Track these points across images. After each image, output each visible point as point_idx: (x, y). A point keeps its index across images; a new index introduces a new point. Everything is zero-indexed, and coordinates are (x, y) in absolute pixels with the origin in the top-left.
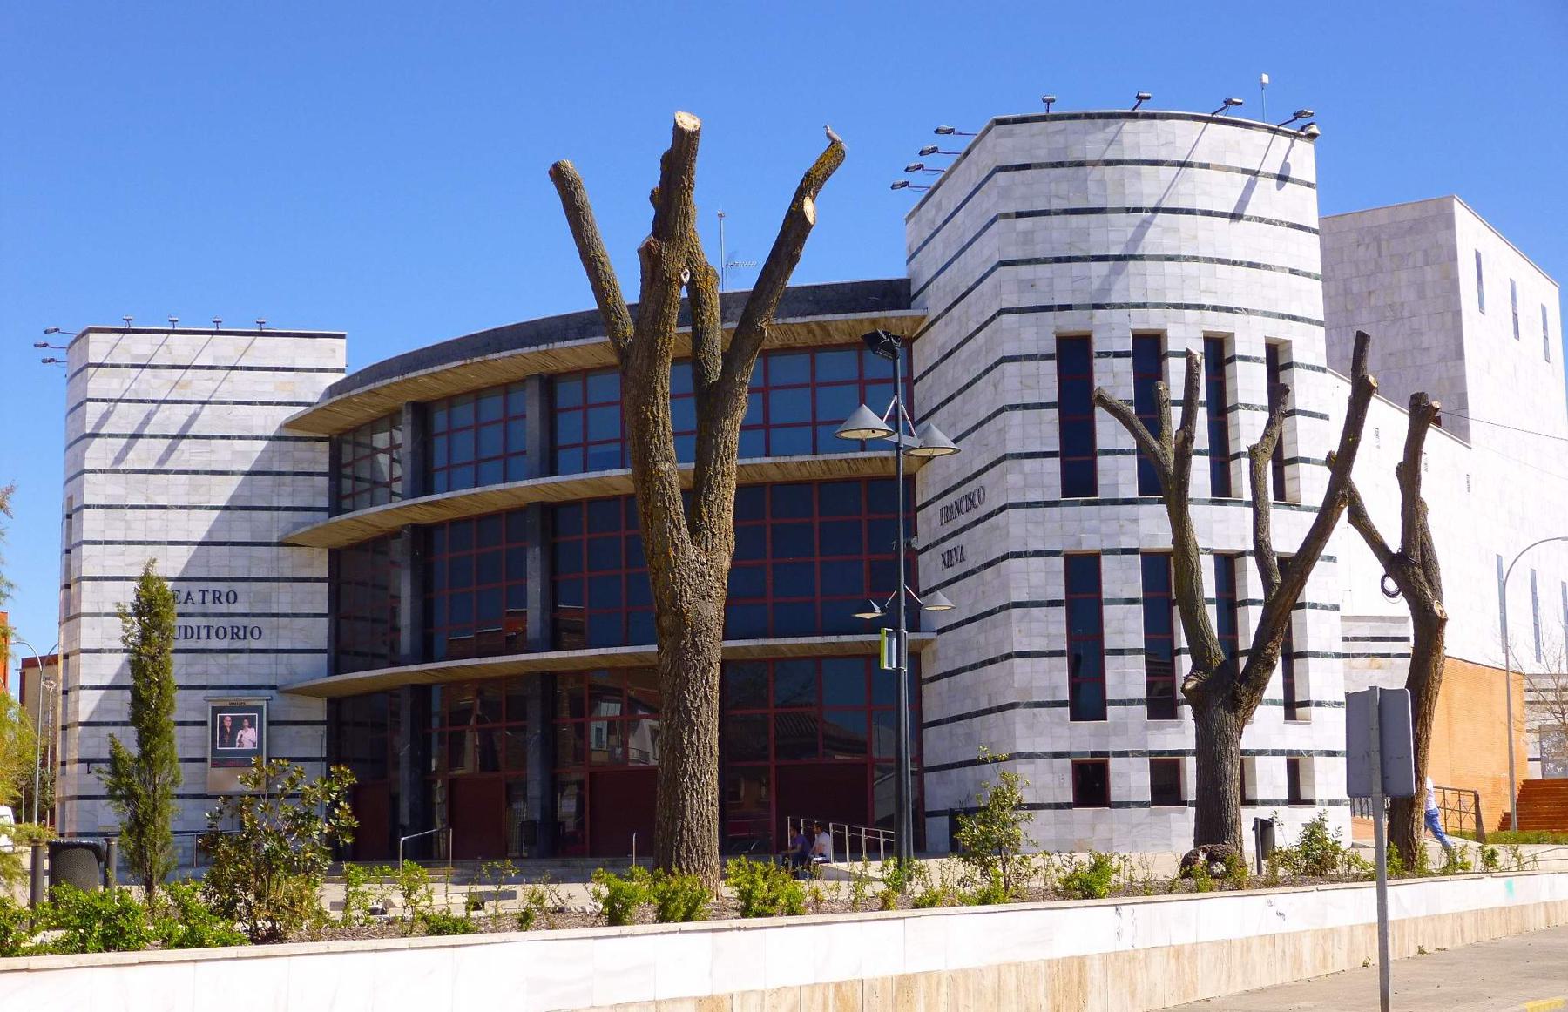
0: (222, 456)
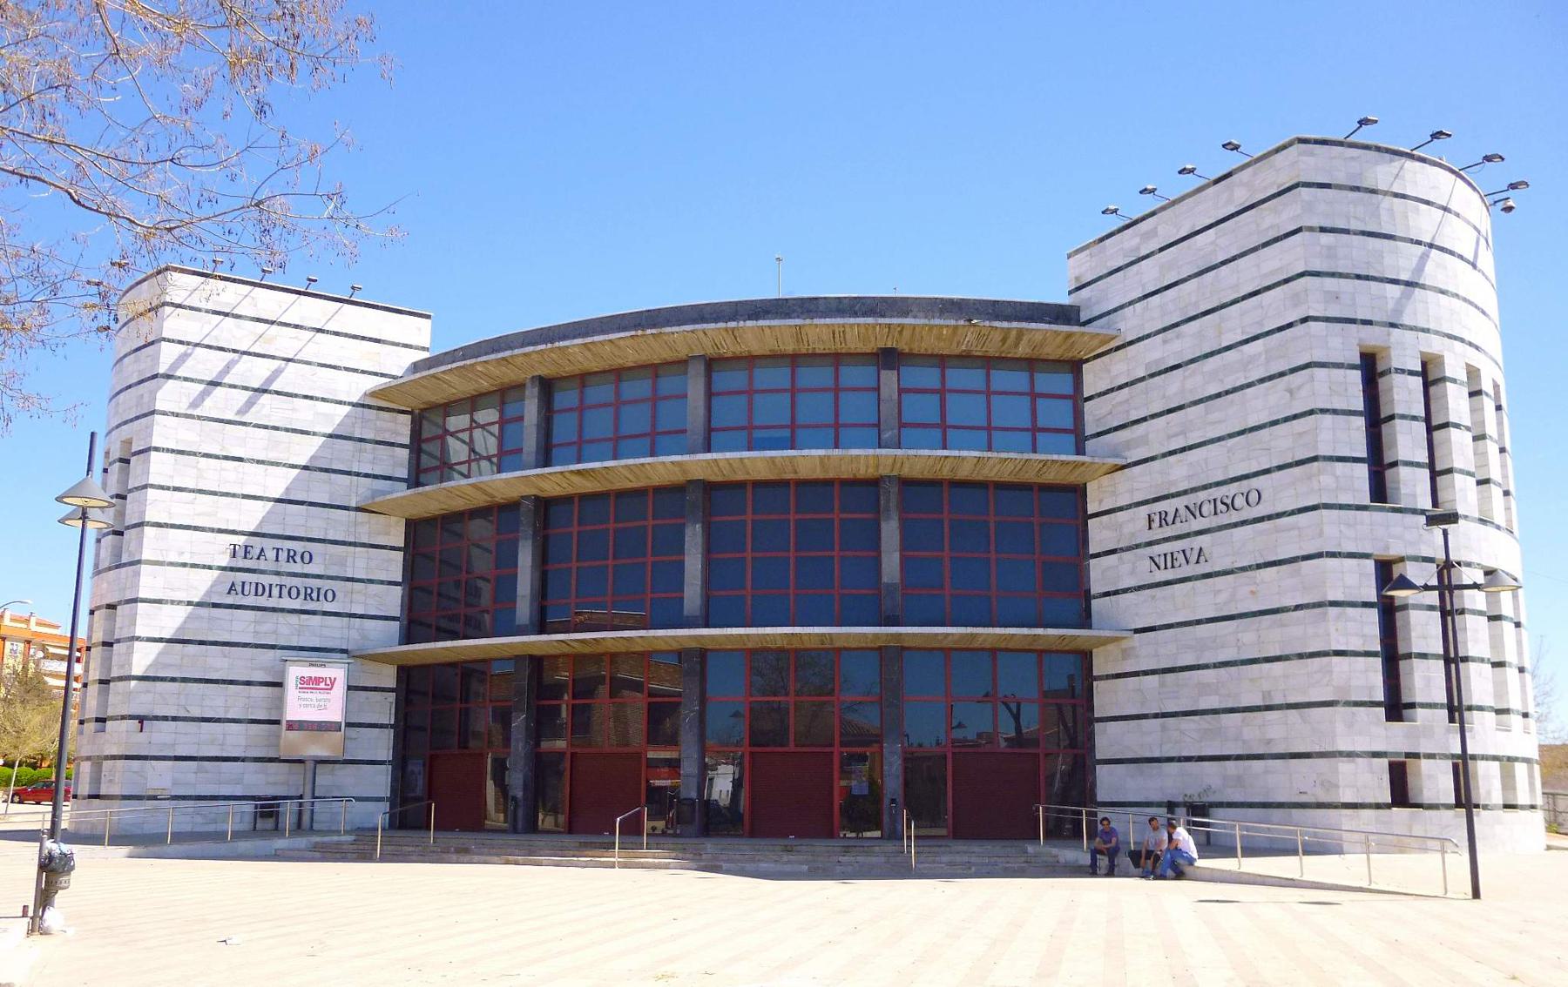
0: (304, 414)
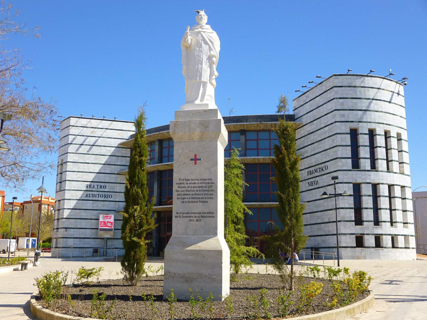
0: (103, 151)
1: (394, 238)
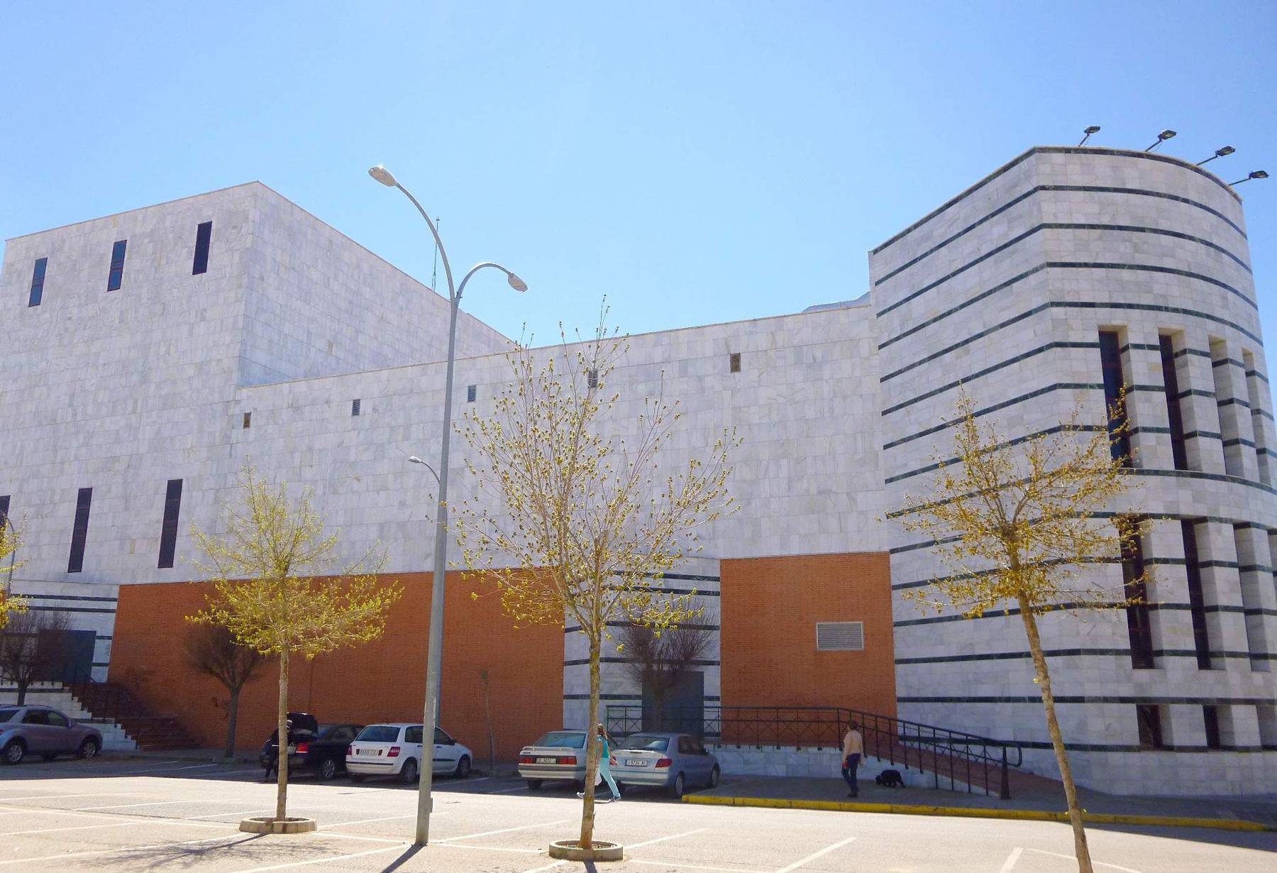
1: (1214, 714)
